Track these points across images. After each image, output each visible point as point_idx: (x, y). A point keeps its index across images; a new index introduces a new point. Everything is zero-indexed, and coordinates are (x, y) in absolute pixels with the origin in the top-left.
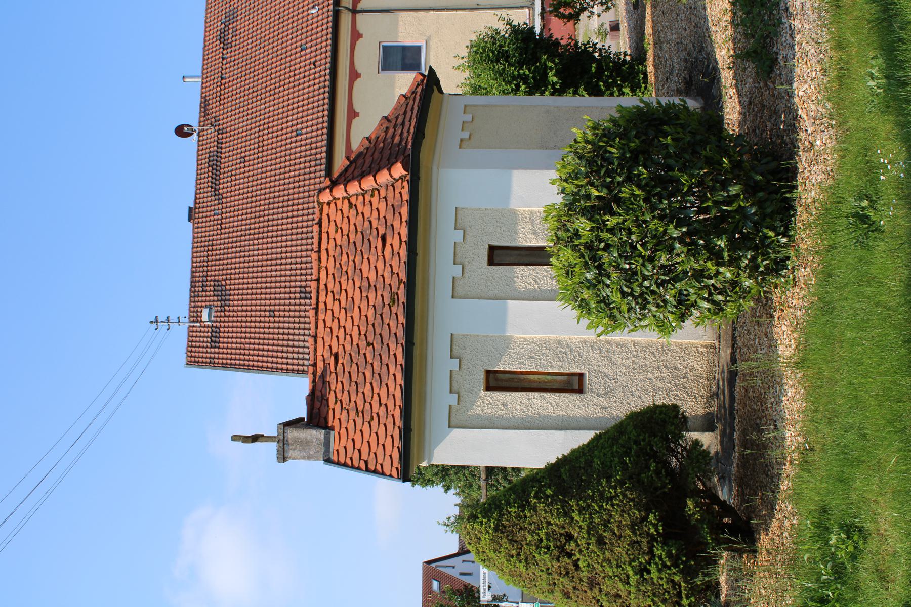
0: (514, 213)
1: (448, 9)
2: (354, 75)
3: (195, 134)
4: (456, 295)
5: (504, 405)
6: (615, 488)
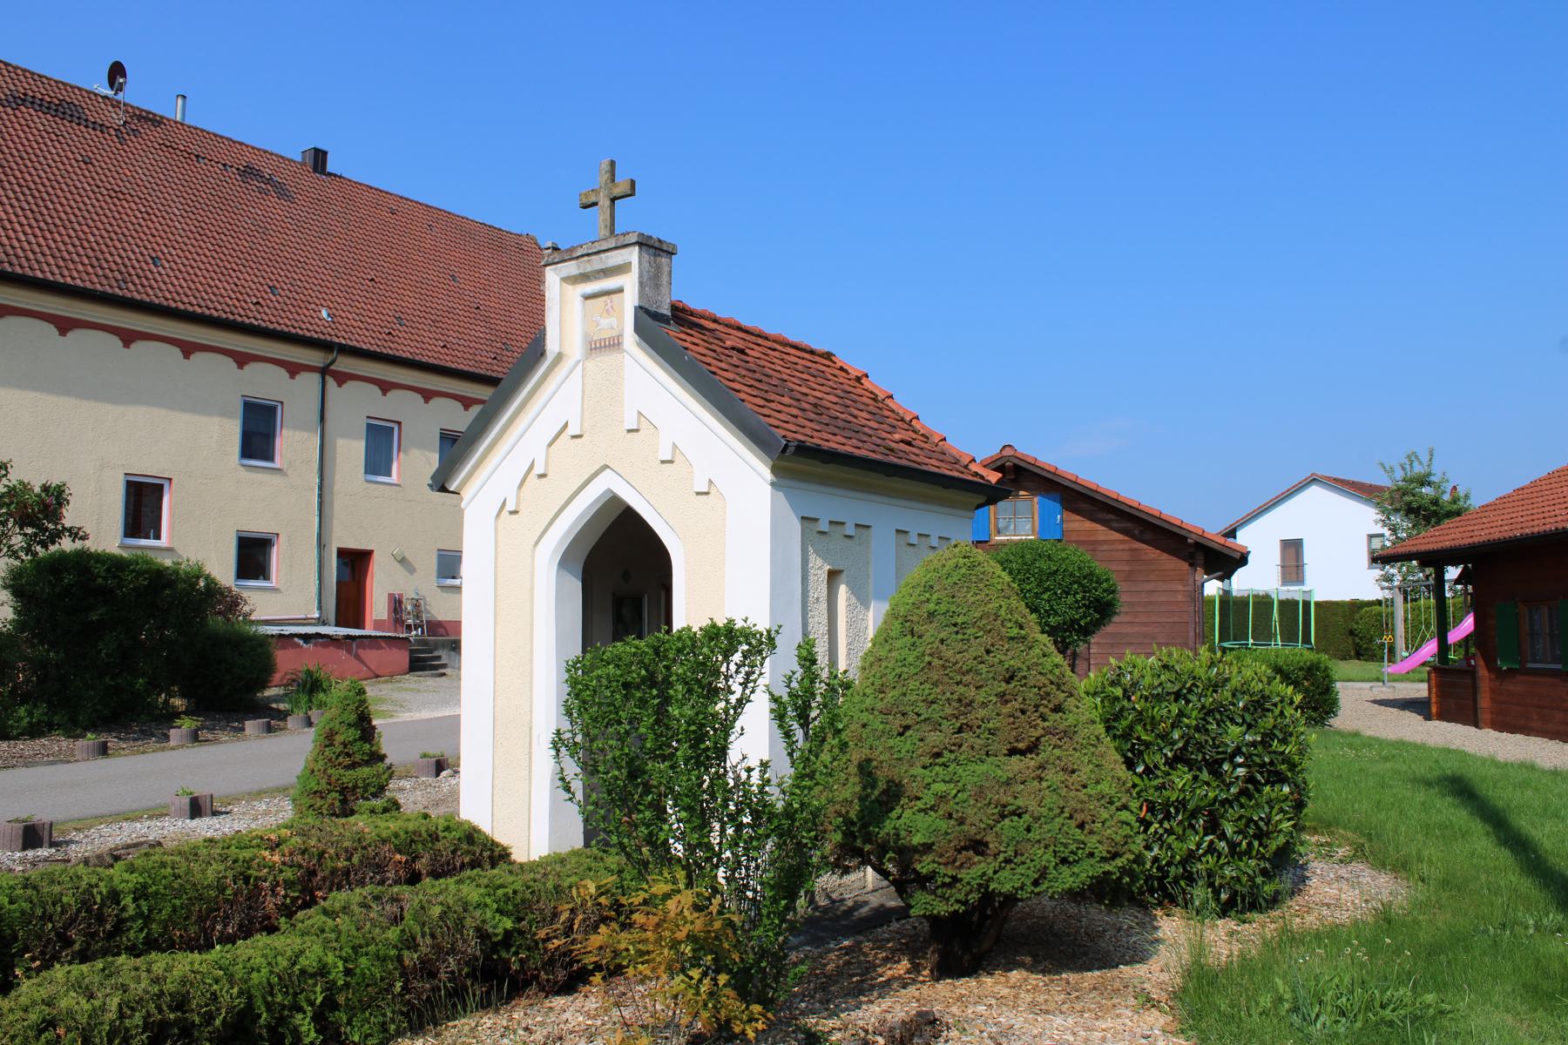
1: (321, 504)
2: (242, 360)
3: (110, 93)
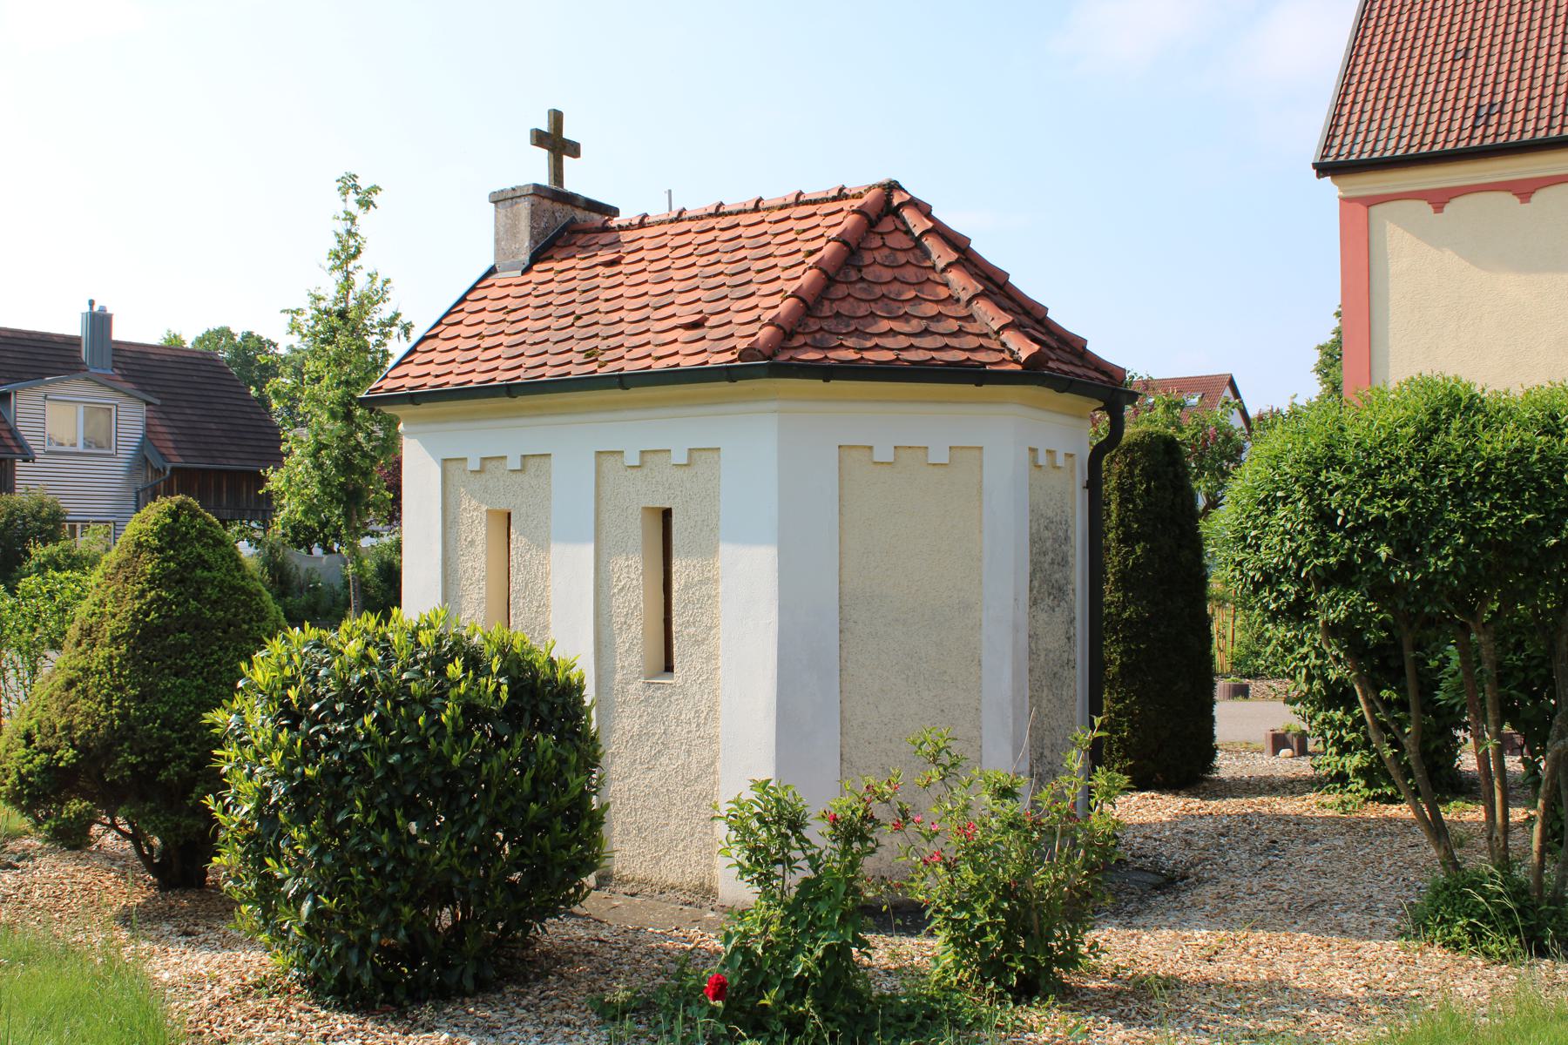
0: (714, 551)
4: (603, 457)
5: (472, 543)
6: (120, 707)
